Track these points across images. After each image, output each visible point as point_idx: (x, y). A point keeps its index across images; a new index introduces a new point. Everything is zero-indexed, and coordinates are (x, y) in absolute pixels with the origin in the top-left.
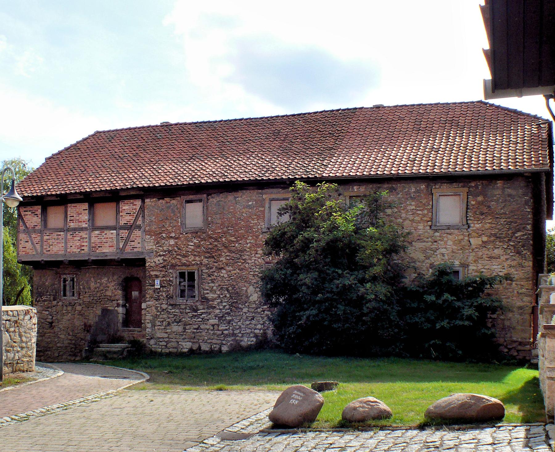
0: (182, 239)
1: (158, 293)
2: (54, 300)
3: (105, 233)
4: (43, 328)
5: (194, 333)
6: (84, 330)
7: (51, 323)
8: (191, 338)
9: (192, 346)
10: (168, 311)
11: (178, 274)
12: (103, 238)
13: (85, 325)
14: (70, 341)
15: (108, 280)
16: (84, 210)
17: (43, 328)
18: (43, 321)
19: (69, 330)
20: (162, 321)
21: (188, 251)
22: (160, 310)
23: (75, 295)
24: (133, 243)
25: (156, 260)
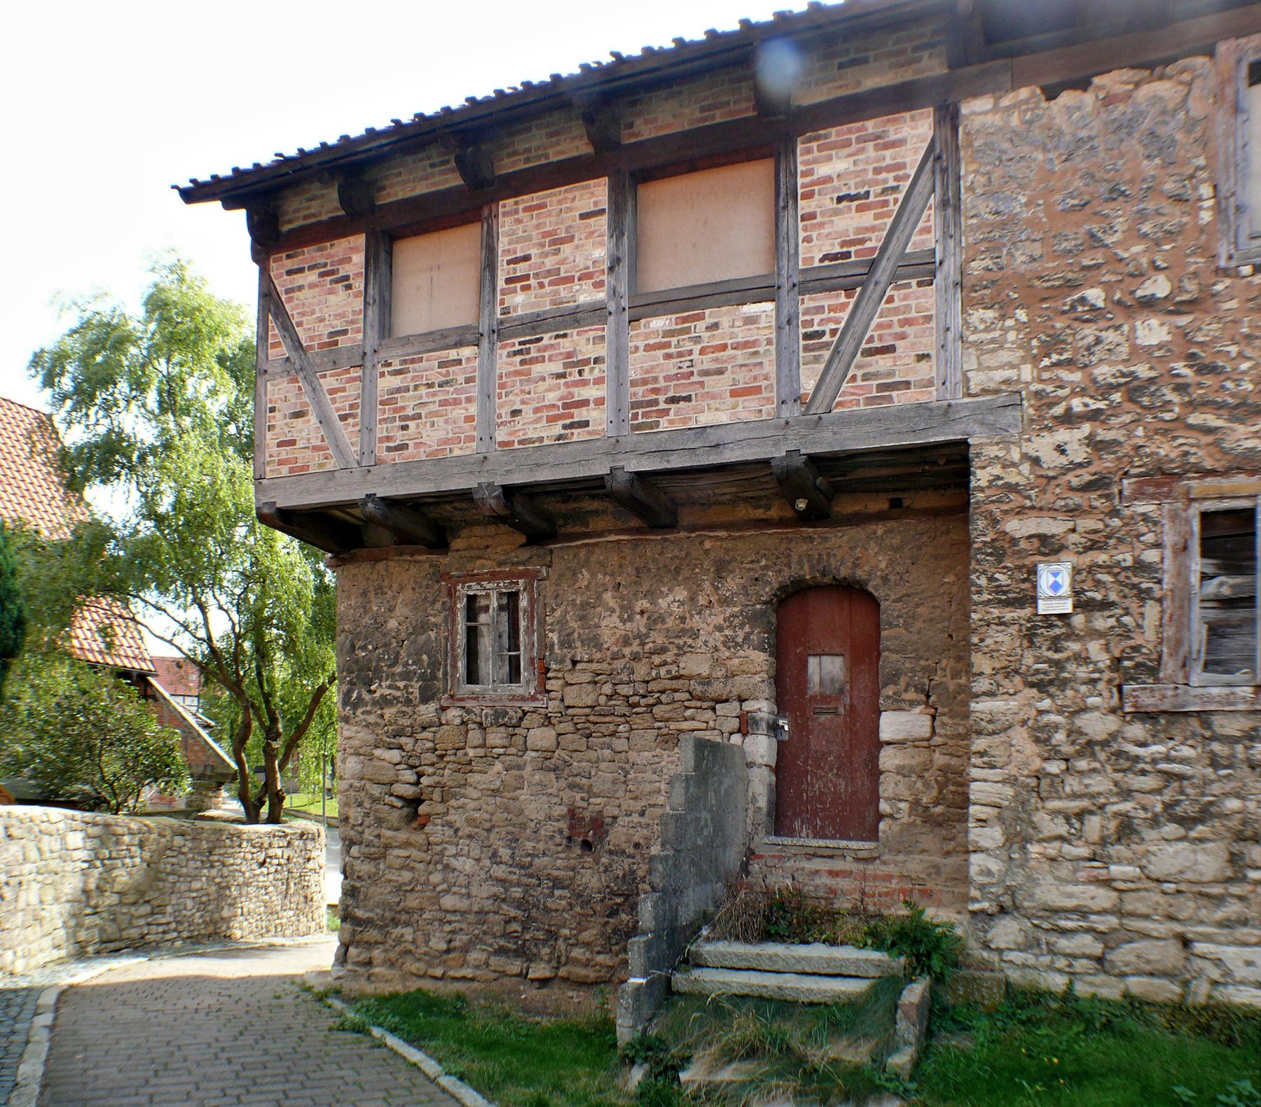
0: (1233, 304)
1: (1055, 644)
2: (425, 699)
3: (709, 321)
4: (380, 821)
6: (569, 839)
7: (415, 802)
10: (1120, 754)
11: (1196, 526)
12: (662, 398)
13: (572, 813)
14: (498, 890)
15: (692, 599)
16: (584, 216)
17: (380, 821)
18: (376, 791)
19: (493, 836)
20: (1081, 815)
22: (1067, 749)
23: (524, 674)
24: (881, 363)
25: (1043, 446)
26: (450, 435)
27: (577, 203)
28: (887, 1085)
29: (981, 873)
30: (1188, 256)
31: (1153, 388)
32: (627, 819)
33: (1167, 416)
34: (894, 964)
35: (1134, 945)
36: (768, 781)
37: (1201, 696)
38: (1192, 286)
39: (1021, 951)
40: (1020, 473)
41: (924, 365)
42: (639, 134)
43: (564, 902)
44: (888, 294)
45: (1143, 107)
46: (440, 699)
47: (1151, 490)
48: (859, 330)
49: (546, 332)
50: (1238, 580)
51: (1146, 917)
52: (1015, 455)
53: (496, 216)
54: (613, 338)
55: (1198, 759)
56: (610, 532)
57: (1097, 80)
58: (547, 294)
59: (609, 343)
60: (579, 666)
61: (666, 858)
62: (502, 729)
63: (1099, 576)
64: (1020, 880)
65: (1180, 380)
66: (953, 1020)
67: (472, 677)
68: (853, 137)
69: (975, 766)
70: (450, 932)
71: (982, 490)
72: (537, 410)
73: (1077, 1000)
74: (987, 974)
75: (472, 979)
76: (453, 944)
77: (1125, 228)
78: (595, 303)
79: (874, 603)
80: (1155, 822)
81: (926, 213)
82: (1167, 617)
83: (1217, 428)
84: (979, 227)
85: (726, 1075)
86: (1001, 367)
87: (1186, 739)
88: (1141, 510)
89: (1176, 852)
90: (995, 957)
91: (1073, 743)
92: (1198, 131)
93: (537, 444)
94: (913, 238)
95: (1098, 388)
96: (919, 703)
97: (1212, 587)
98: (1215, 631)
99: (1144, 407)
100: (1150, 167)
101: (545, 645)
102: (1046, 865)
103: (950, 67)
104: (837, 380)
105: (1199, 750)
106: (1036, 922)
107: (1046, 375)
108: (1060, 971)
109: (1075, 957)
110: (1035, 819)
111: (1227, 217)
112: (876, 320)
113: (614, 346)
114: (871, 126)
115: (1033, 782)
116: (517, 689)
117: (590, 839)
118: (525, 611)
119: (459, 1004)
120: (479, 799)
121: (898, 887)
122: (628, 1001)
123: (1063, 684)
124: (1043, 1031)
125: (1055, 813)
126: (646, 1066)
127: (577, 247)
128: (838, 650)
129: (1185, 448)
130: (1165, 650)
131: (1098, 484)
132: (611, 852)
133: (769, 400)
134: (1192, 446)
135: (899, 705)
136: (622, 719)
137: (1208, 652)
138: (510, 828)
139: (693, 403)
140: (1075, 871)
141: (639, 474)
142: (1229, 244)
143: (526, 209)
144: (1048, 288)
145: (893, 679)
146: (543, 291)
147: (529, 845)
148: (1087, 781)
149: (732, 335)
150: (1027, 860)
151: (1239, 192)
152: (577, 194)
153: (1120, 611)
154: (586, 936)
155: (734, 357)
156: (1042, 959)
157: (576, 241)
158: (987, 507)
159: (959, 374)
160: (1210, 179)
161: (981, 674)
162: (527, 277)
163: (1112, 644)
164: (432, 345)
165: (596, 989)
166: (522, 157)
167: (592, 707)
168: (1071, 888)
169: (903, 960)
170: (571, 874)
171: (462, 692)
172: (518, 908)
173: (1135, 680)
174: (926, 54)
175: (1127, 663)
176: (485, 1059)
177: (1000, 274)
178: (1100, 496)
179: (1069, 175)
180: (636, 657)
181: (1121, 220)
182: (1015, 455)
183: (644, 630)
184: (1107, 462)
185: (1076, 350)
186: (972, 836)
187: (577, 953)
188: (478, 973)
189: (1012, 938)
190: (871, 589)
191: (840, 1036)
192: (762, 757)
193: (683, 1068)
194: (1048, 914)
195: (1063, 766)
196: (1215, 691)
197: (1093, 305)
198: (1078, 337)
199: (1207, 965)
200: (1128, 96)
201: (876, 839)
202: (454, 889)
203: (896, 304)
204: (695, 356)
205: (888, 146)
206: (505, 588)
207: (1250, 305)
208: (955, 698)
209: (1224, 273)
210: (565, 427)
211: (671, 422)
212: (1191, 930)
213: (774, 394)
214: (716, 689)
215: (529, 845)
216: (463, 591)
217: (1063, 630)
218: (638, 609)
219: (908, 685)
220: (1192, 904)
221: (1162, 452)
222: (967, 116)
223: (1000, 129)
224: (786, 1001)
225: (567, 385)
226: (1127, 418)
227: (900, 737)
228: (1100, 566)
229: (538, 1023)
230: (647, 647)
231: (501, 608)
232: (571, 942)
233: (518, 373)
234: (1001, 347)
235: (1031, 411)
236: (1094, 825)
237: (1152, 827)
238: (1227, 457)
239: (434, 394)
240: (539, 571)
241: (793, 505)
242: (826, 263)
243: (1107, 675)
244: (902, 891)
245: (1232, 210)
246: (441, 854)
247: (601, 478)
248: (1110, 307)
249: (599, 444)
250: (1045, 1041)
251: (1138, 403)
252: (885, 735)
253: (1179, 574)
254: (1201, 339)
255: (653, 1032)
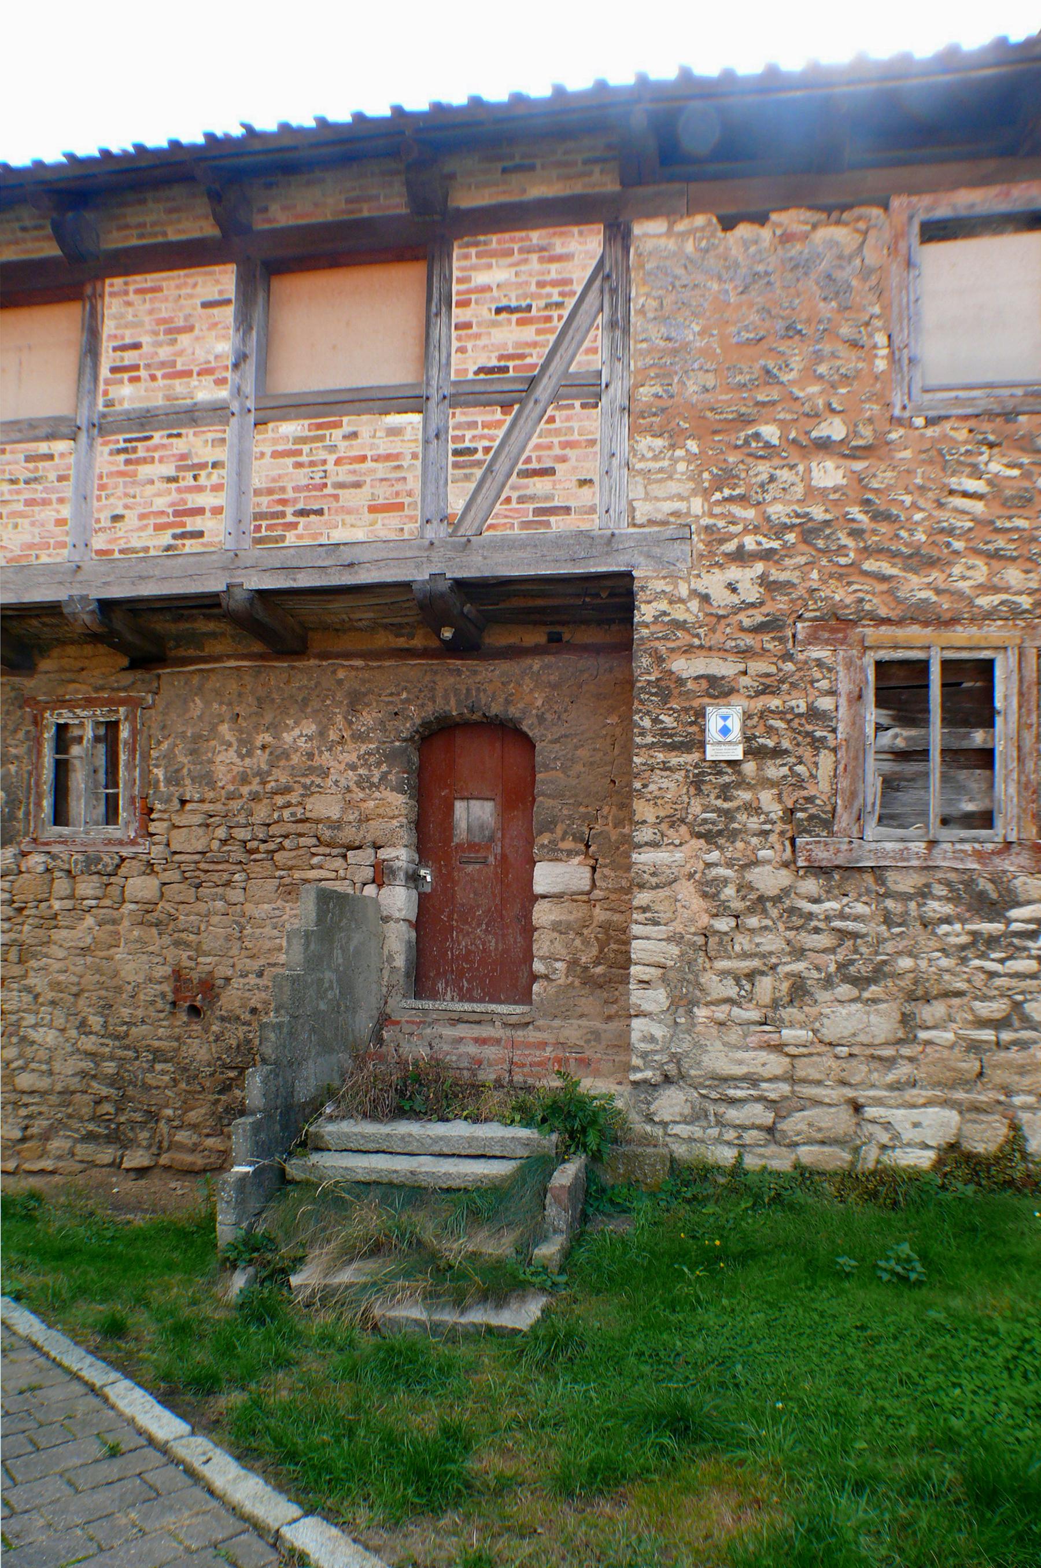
0: (907, 454)
1: (725, 792)
3: (347, 429)
5: (975, 1047)
6: (174, 1004)
8: (961, 1082)
9: (959, 1135)
10: (792, 911)
12: (289, 510)
13: (177, 975)
14: (87, 1065)
16: (206, 305)
19: (81, 1002)
21: (950, 532)
22: (737, 905)
23: (123, 815)
24: (539, 486)
25: (714, 583)
26: (37, 540)
27: (199, 290)
28: (534, 1279)
29: (644, 1039)
30: (863, 402)
31: (828, 531)
32: (241, 980)
33: (843, 561)
34: (545, 1142)
35: (805, 1113)
36: (406, 937)
37: (876, 852)
38: (867, 434)
39: (687, 1123)
40: (688, 610)
41: (586, 490)
42: (275, 220)
43: (166, 1078)
44: (549, 413)
45: (820, 250)
46: (19, 843)
47: (826, 635)
48: (515, 451)
49: (156, 430)
50: (913, 732)
51: (819, 1083)
52: (683, 591)
53: (102, 296)
54: (236, 441)
55: (872, 916)
56: (229, 657)
57: (774, 217)
58: (159, 388)
59: (231, 446)
60: (189, 807)
61: (280, 1025)
62: (95, 877)
63: (771, 722)
64: (686, 1046)
65: (855, 526)
66: (611, 1201)
67: (60, 817)
68: (516, 247)
69: (637, 922)
70: (26, 1117)
71: (646, 625)
72: (142, 516)
73: (746, 1173)
74: (650, 1150)
75: (52, 1173)
76: (29, 1132)
77: (801, 367)
78: (215, 402)
79: (528, 744)
80: (828, 983)
81: (592, 333)
82: (841, 767)
83: (892, 577)
84: (649, 351)
85: (345, 1277)
86: (670, 498)
87: (860, 895)
88: (816, 655)
89: (849, 1014)
90: (659, 1131)
91: (743, 898)
92: (873, 280)
93: (141, 555)
94: (578, 358)
95: (772, 527)
96: (577, 854)
97: (886, 739)
98: (890, 784)
99: (819, 550)
100: (827, 309)
101: (149, 782)
102: (714, 1031)
103: (623, 184)
104: (489, 501)
105: (873, 907)
106: (703, 1092)
107: (717, 510)
108: (729, 1143)
109: (745, 1128)
110: (702, 981)
111: (901, 368)
112: (535, 440)
113: (235, 450)
114: (536, 236)
115: (701, 940)
116: (113, 832)
117: (198, 1004)
118: (126, 743)
119: (33, 1204)
120: (65, 959)
121: (553, 1055)
122: (228, 1194)
123: (733, 835)
124: (709, 1209)
125: (724, 973)
126: (251, 1270)
127: (197, 338)
128: (488, 794)
129: (860, 595)
130: (839, 802)
131: (771, 626)
132: (223, 1019)
133: (412, 518)
134: (868, 593)
135: (555, 855)
136: (238, 867)
137: (882, 806)
138: (103, 993)
139: (326, 517)
140: (745, 1036)
141: (260, 592)
142: (903, 394)
143: (139, 291)
144: (720, 421)
145: (549, 826)
146: (155, 384)
147: (125, 1012)
148: (758, 940)
149: (372, 446)
150: (694, 1025)
151: (912, 344)
152: (200, 279)
153: (793, 760)
154: (193, 1116)
155: (374, 471)
156: (709, 1131)
157: (196, 332)
158: (652, 644)
159: (624, 502)
160: (885, 328)
161: (644, 822)
162: (136, 367)
163: (785, 794)
164: (18, 436)
165: (200, 1180)
166: (135, 232)
167: (203, 853)
168: (740, 1055)
169: (554, 1137)
170: (175, 1044)
171: (46, 834)
172: (111, 1085)
173: (809, 832)
174: (597, 169)
175: (800, 815)
176: (55, 1270)
177: (670, 402)
178: (773, 638)
179: (744, 308)
180: (255, 798)
181: (797, 358)
182: (683, 591)
183: (264, 767)
184: (781, 604)
185: (750, 486)
186: (633, 999)
187: (182, 1136)
188: (61, 1164)
189: (677, 1109)
190: (525, 729)
191: (481, 1225)
192: (400, 910)
193: (294, 1270)
194: (716, 1083)
195: (733, 924)
196: (889, 846)
197: (767, 442)
198: (751, 473)
199: (877, 1130)
200: (805, 236)
201: (530, 1002)
202: (33, 1065)
203: (557, 424)
204: (330, 466)
205: (553, 259)
206: (101, 714)
207: (923, 456)
208: (618, 848)
209: (899, 422)
210: (175, 537)
211: (300, 537)
212: (862, 1095)
213: (419, 513)
214: (348, 834)
215: (125, 1012)
216: (51, 718)
217: (733, 778)
218: (259, 744)
219: (565, 833)
220: (864, 1068)
221: (837, 598)
222: (639, 238)
223: (675, 254)
224: (419, 1187)
225: (179, 490)
226: (802, 560)
227: (556, 890)
228: (772, 712)
229: (129, 1222)
230: (269, 787)
231: (97, 739)
232: (175, 1124)
233: (122, 474)
234: (670, 477)
235: (701, 546)
236: (765, 986)
237: (825, 988)
238: (901, 607)
239: (18, 492)
240: (143, 699)
241: (438, 634)
242: (482, 376)
243: (779, 827)
244: (559, 1061)
245: (905, 361)
246: (17, 1024)
247: (216, 595)
248: (784, 445)
249: (214, 557)
250: (712, 1220)
251: (814, 546)
252: (538, 888)
253: (854, 724)
254: (876, 486)
255: (260, 1230)
